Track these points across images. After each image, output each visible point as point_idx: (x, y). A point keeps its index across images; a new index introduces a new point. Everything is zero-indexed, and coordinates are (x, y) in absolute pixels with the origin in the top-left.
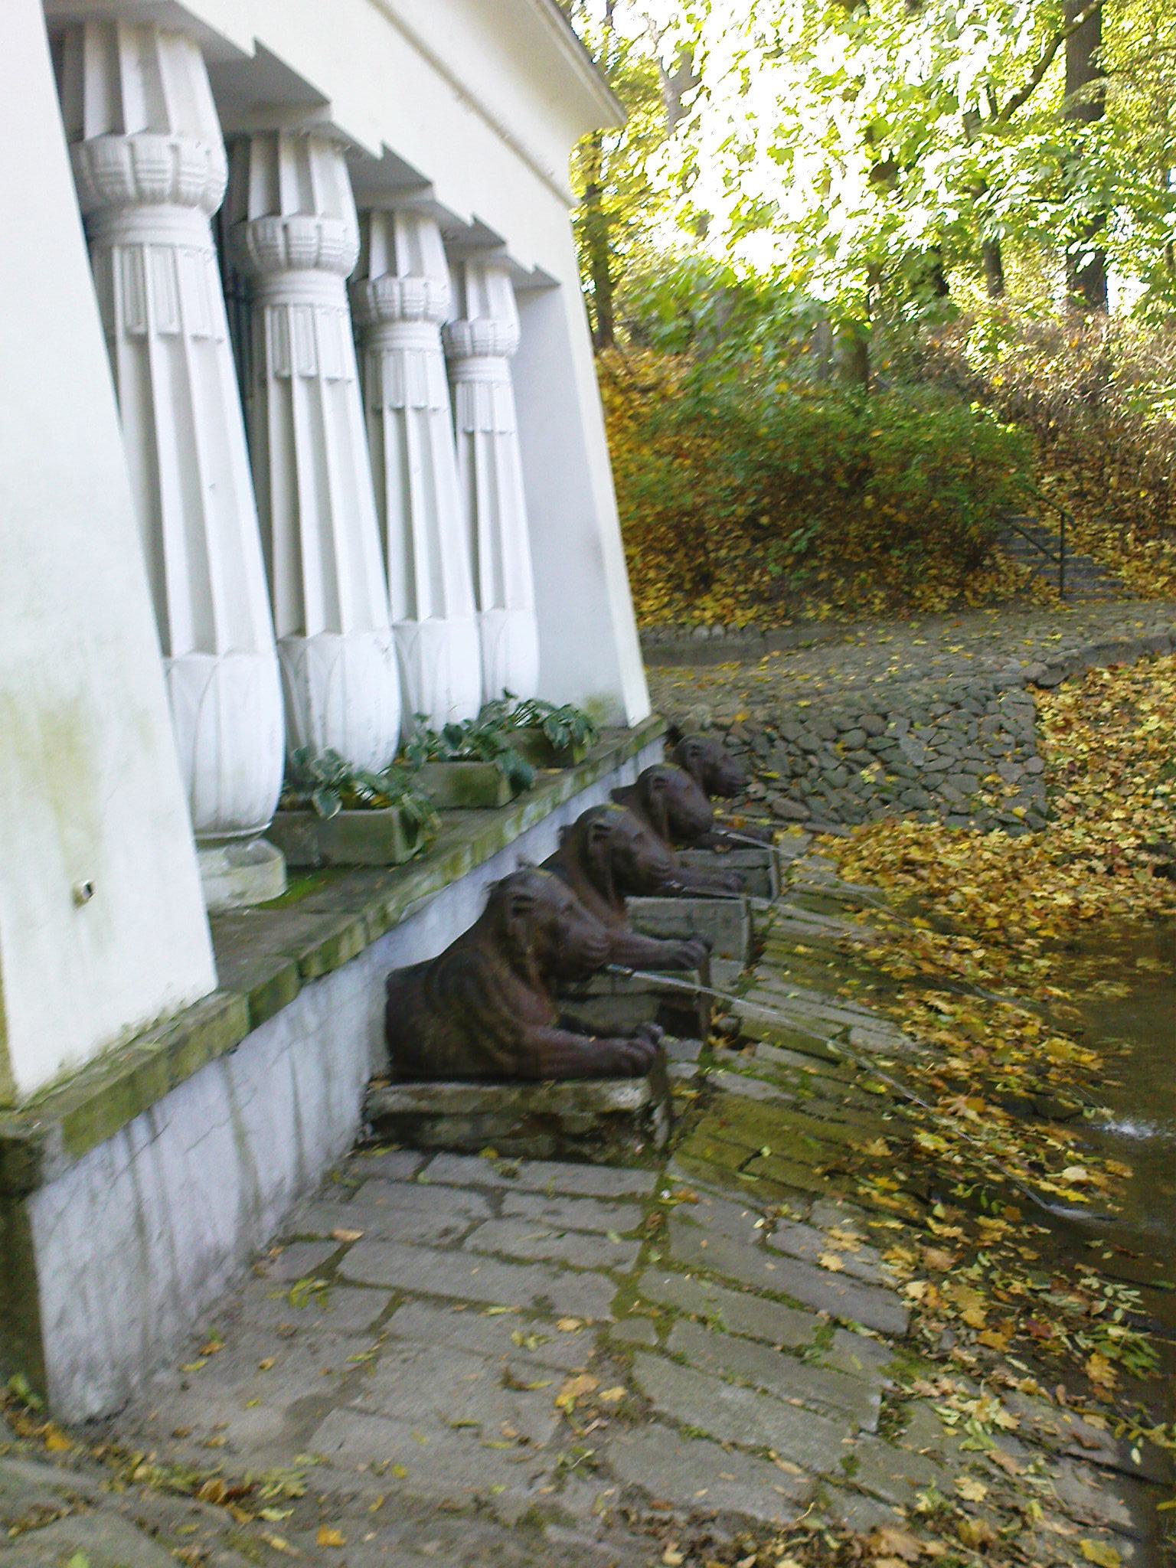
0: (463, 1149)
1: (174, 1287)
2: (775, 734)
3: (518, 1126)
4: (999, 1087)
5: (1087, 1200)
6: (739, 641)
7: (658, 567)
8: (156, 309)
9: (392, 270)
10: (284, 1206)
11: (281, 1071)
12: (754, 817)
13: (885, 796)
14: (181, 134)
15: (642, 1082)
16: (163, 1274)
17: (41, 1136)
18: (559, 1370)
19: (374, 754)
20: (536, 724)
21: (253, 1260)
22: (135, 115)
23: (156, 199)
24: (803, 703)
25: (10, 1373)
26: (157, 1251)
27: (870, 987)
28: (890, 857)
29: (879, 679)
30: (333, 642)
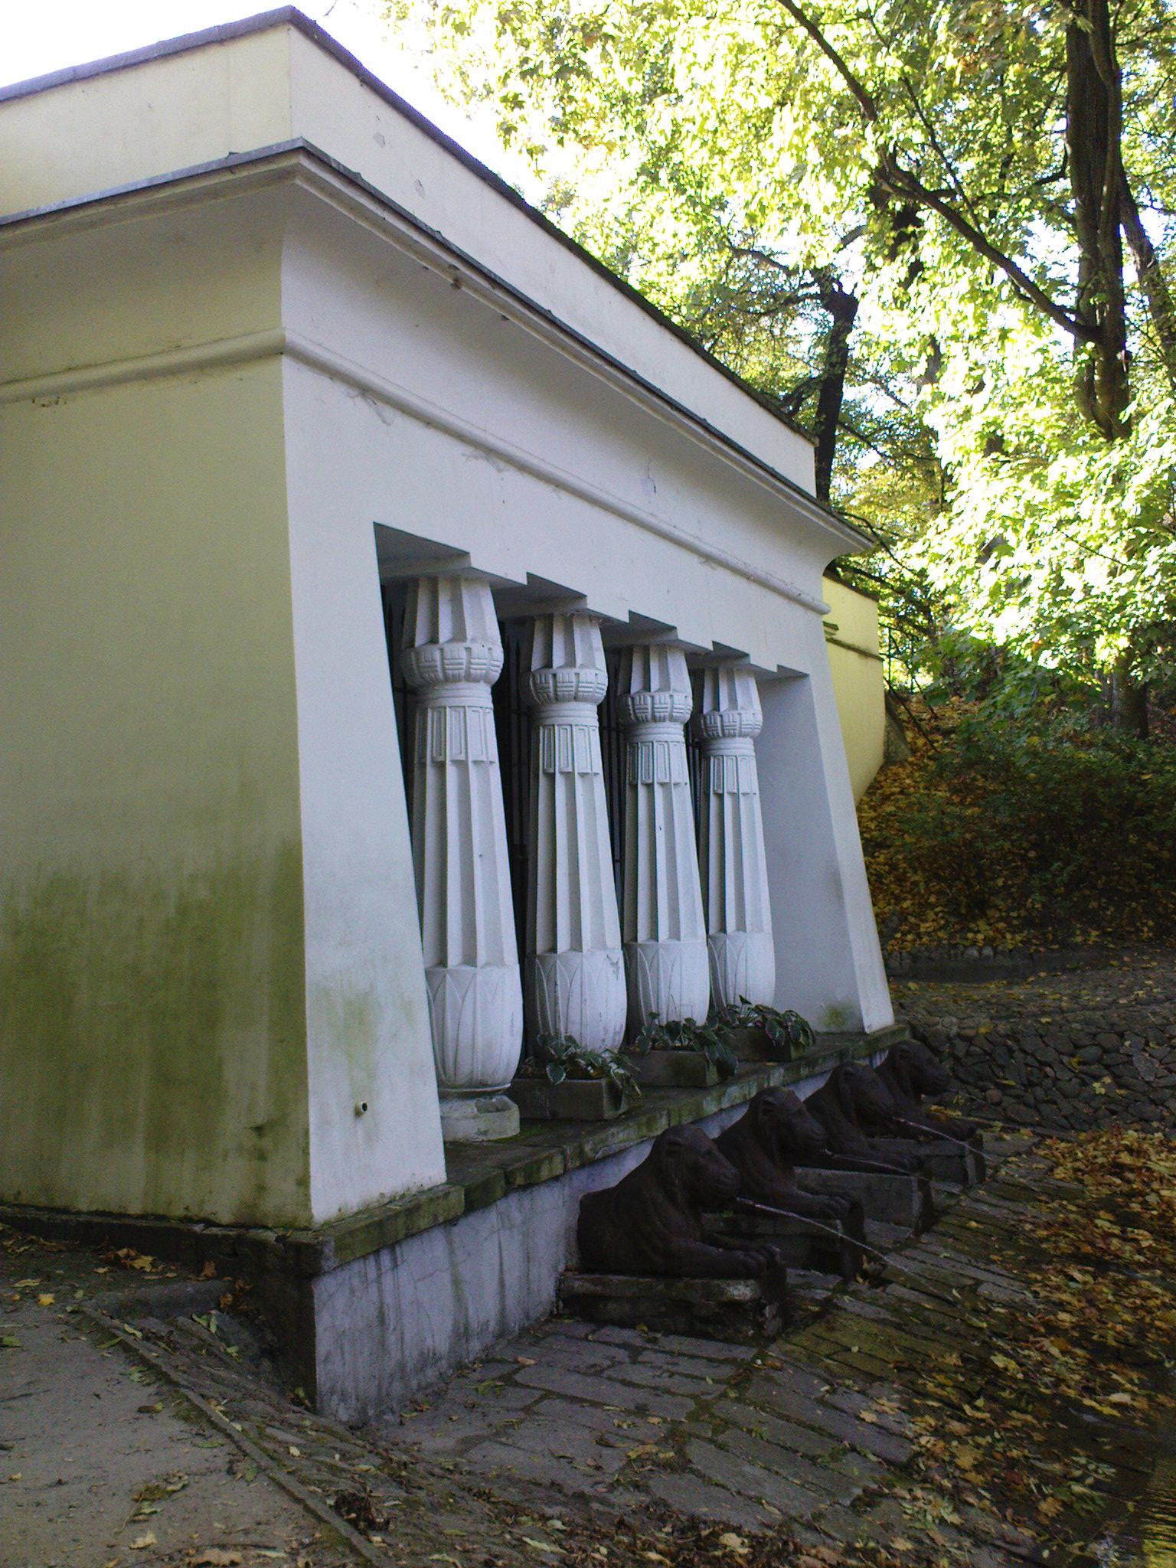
0: (623, 1324)
1: (402, 1366)
2: (1015, 1047)
3: (663, 1309)
4: (1095, 1337)
5: (1118, 1415)
6: (1007, 962)
7: (940, 893)
8: (451, 748)
9: (647, 687)
10: (489, 1339)
11: (490, 1249)
12: (989, 1119)
13: (1113, 1107)
14: (473, 640)
15: (751, 1282)
16: (396, 1355)
17: (322, 1244)
18: (638, 1441)
19: (604, 1040)
20: (760, 1027)
21: (461, 1368)
22: (445, 632)
23: (456, 679)
24: (1044, 1020)
25: (294, 1387)
26: (392, 1338)
27: (1022, 1257)
28: (1100, 1160)
29: (1122, 1001)
30: (575, 957)
